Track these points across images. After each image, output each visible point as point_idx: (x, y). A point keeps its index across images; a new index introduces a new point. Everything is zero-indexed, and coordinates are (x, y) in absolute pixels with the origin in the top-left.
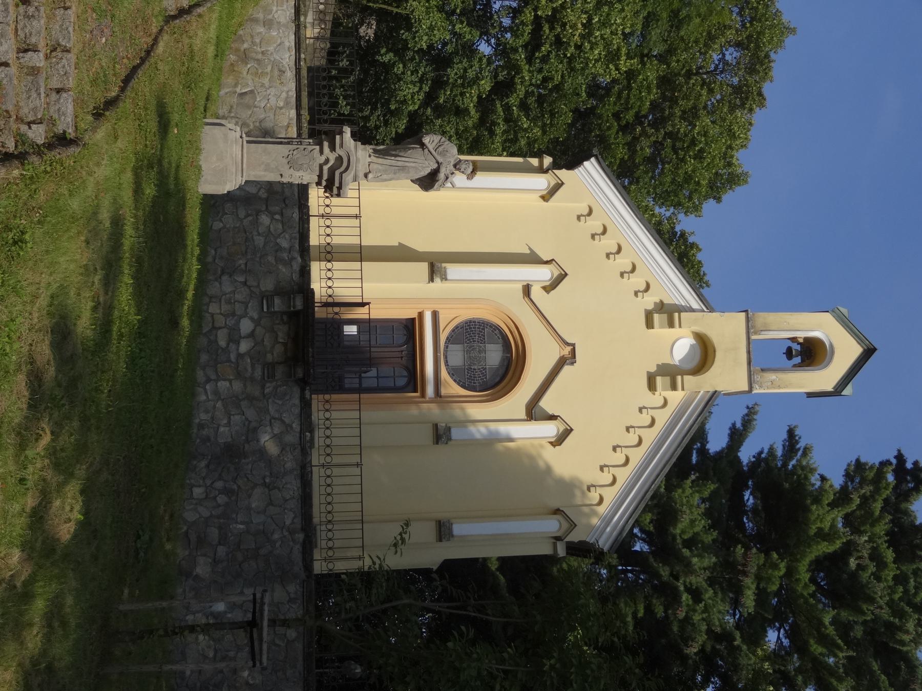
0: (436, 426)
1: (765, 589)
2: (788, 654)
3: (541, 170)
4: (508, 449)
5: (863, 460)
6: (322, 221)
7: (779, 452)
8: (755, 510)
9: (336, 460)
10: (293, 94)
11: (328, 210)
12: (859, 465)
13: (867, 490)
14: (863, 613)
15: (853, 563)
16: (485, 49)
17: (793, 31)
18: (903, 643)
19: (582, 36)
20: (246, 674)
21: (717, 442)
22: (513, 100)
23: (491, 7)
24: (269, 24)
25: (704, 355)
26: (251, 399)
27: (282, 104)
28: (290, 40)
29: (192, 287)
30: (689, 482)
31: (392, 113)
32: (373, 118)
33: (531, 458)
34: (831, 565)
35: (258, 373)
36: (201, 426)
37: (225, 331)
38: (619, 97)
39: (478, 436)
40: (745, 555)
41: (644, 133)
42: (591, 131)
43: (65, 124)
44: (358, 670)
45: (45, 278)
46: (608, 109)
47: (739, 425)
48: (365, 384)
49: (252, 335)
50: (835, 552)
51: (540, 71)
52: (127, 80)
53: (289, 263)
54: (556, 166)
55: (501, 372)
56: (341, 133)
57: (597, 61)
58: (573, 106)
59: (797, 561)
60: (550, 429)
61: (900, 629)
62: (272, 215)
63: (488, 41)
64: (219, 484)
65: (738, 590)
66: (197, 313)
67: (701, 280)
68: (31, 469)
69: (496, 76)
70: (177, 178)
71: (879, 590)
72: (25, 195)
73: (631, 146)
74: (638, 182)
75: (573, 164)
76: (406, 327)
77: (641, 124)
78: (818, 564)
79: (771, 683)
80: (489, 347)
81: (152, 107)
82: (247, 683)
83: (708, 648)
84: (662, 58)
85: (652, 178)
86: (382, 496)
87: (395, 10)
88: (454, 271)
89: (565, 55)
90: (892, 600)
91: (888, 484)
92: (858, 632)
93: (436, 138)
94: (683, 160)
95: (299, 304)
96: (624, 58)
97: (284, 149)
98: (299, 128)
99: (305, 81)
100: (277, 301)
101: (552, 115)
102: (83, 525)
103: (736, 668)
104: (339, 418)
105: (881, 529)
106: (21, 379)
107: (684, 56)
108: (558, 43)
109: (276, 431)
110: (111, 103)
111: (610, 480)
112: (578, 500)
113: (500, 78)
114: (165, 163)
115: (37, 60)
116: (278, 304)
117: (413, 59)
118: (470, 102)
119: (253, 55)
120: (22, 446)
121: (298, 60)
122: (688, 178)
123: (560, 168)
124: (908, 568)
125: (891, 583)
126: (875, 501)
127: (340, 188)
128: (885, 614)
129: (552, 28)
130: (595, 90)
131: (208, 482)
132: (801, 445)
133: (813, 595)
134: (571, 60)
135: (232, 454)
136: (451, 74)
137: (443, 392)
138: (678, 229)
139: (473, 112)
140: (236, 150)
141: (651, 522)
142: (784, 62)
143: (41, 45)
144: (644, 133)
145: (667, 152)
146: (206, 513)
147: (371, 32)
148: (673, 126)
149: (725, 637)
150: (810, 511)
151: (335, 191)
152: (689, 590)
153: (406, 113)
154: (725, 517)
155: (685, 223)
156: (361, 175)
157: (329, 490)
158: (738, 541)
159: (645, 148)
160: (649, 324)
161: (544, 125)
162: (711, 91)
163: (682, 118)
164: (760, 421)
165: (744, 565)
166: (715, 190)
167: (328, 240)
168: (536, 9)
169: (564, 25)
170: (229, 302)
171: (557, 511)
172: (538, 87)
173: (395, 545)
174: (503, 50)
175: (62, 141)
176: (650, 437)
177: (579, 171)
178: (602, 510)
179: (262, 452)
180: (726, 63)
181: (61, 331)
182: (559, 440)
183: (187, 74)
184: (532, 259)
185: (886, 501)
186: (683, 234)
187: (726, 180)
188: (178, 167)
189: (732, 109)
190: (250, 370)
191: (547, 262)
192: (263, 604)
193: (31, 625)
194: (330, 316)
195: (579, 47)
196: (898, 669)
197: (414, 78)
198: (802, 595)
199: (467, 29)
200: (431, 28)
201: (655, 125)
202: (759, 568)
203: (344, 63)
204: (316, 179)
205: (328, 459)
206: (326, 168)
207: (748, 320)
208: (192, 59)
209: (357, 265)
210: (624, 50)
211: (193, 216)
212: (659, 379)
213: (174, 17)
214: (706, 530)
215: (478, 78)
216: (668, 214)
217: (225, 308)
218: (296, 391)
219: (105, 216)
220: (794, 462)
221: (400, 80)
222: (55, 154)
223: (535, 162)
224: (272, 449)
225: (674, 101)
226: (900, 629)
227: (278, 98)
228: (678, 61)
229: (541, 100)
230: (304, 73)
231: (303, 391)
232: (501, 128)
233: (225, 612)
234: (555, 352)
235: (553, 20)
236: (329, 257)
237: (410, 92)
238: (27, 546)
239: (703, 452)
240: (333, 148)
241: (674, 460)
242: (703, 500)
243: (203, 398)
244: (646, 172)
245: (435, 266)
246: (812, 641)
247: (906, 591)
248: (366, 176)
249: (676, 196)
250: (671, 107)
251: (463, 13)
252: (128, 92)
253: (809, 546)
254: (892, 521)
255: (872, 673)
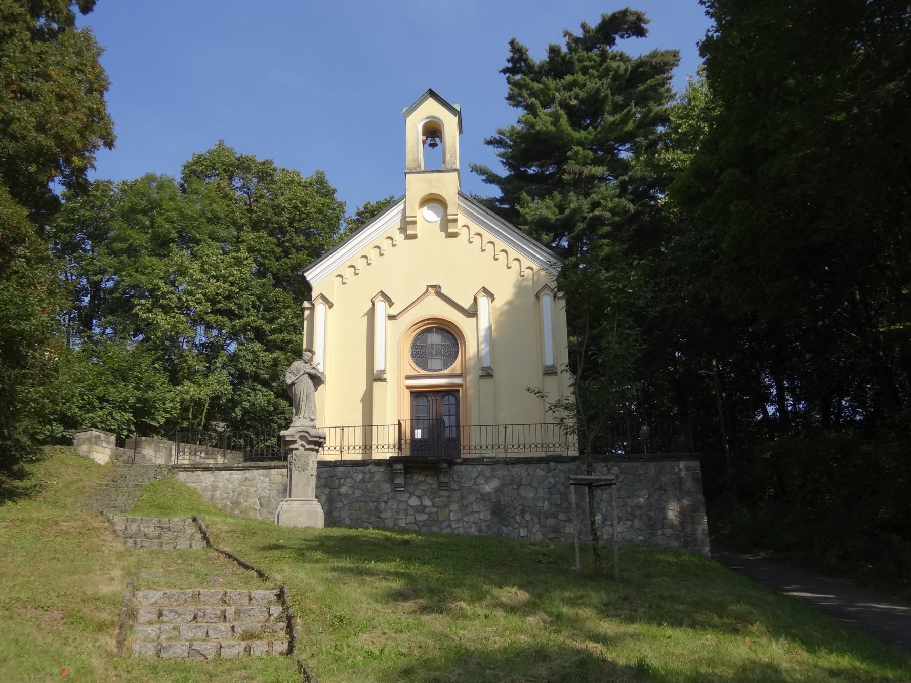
0: (481, 377)
1: (592, 160)
2: (635, 144)
3: (312, 308)
4: (496, 329)
5: (507, 95)
6: (345, 452)
7: (502, 150)
8: (541, 166)
9: (502, 441)
10: (261, 472)
11: (338, 448)
12: (510, 98)
13: (525, 93)
14: (606, 96)
15: (574, 102)
16: (233, 347)
17: (221, 142)
18: (626, 70)
19: (225, 282)
20: (642, 500)
21: (495, 192)
22: (267, 328)
23: (205, 343)
24: (214, 488)
25: (433, 200)
26: (462, 498)
27: (267, 479)
28: (225, 474)
29: (384, 533)
30: (521, 210)
31: (276, 409)
32: (280, 421)
33: (501, 314)
34: (576, 117)
35: (445, 493)
36: (480, 530)
37: (417, 515)
38: (265, 257)
39: (487, 349)
40: (569, 173)
41: (290, 241)
42: (289, 276)
43: (271, 595)
44: (645, 428)
45: (364, 605)
46: (274, 265)
47: (484, 177)
48: (454, 423)
49: (420, 498)
50: (567, 114)
51: (248, 310)
52: (247, 567)
53: (372, 474)
54: (310, 299)
55: (446, 334)
56: (284, 437)
57: (241, 272)
58: (271, 288)
59: (573, 138)
60: (483, 301)
61: (617, 71)
62: (340, 485)
63: (228, 345)
64: (518, 518)
65: (592, 177)
66: (403, 531)
67: (389, 202)
68: (479, 612)
69: (251, 339)
70: (312, 541)
71: (591, 85)
72: (313, 616)
73: (298, 249)
74: (323, 245)
75: (308, 288)
76: (416, 397)
77: (284, 243)
78: (576, 124)
79: (653, 156)
80: (429, 342)
81: (265, 553)
82: (648, 499)
83: (631, 197)
84: (240, 229)
85: (319, 234)
86: (524, 415)
87: (207, 407)
88: (378, 366)
89: (238, 293)
90: (598, 76)
91: (522, 79)
92: (619, 98)
93: (288, 375)
94: (308, 215)
95: (399, 467)
96: (239, 254)
97: (295, 473)
98: (284, 467)
99: (253, 464)
100: (397, 481)
101: (277, 302)
102: (521, 587)
103: (643, 178)
104: (476, 440)
105: (551, 83)
106: (425, 618)
107: (238, 214)
108: (229, 298)
109: (483, 481)
110: (261, 574)
111: (516, 262)
112: (530, 283)
113: (252, 336)
114: (301, 547)
115: (230, 611)
116: (399, 480)
117: (240, 395)
118: (268, 357)
119: (235, 498)
120: (465, 616)
121: (239, 469)
122: (320, 211)
123: (311, 296)
124: (578, 66)
125: (587, 77)
126: (533, 87)
127: (320, 437)
128: (607, 81)
129: (220, 302)
130: (260, 274)
131: (517, 525)
132: (497, 136)
133: (595, 128)
134: (241, 290)
135: (498, 510)
136: (249, 369)
137: (458, 372)
138: (355, 218)
139: (275, 355)
140: (295, 504)
141: (547, 234)
142: (245, 146)
143: (223, 608)
144: (290, 241)
145: (302, 225)
146: (537, 527)
147: (222, 424)
148: (285, 221)
149: (623, 186)
150: (539, 130)
151: (322, 440)
152: (592, 210)
153: (275, 400)
154: (544, 186)
155: (351, 212)
156: (312, 423)
157: (522, 446)
158: (560, 177)
159: (300, 240)
160: (414, 237)
161: (284, 307)
162: (261, 196)
163: (279, 215)
164: (480, 164)
165: (575, 173)
166: (328, 193)
167: (357, 448)
168: (207, 313)
169: (217, 294)
170: (398, 513)
171: (537, 297)
172: (258, 311)
173: (542, 397)
174: (234, 335)
175: (281, 596)
176: (488, 236)
177: (313, 284)
178: (536, 267)
179: (498, 491)
180: (243, 186)
181: (399, 596)
182: (490, 295)
183: (245, 534)
184: (371, 314)
185: (533, 80)
186: (359, 214)
187: (322, 187)
188: (305, 540)
189: (274, 182)
190: (442, 499)
191: (373, 304)
192: (577, 479)
193: (577, 614)
194: (409, 446)
195: (232, 284)
196: (643, 73)
197: (252, 394)
198: (596, 135)
199: (220, 359)
200: (219, 382)
201: (284, 233)
202: (578, 164)
203: (242, 441)
204: (314, 453)
205: (502, 447)
206: (307, 446)
207: (411, 172)
208: (235, 531)
209: (374, 428)
210: (234, 254)
211: (337, 532)
212: (450, 230)
213: (208, 542)
214: (553, 198)
215: (253, 352)
216: (345, 224)
217: (402, 515)
218: (456, 468)
219: (330, 575)
220: (508, 141)
221: (253, 404)
222: (288, 599)
223: (307, 313)
224: (494, 484)
225: (268, 221)
226: (617, 71)
227: (263, 480)
228: (241, 218)
229: (267, 309)
230: (247, 464)
231: (456, 464)
232: (286, 336)
233: (602, 514)
234: (433, 299)
235: (213, 302)
236: (368, 447)
237: (261, 397)
238: (526, 614)
239: (502, 201)
240: (294, 442)
241: (503, 220)
242: (533, 200)
243: (461, 529)
244: (316, 239)
245: (375, 378)
246: (626, 129)
247: (593, 67)
248: (312, 420)
249: (331, 219)
250: (272, 223)
251: (209, 362)
252: (255, 565)
253: (563, 131)
254: (547, 76)
255: (646, 90)
